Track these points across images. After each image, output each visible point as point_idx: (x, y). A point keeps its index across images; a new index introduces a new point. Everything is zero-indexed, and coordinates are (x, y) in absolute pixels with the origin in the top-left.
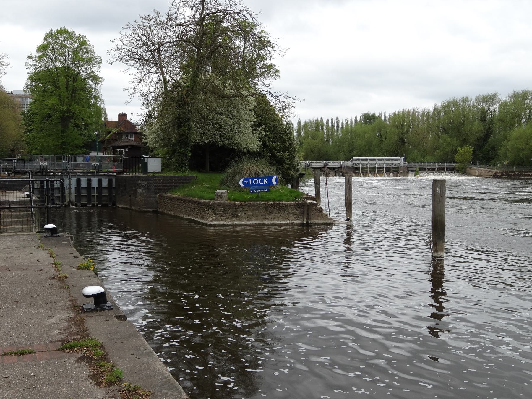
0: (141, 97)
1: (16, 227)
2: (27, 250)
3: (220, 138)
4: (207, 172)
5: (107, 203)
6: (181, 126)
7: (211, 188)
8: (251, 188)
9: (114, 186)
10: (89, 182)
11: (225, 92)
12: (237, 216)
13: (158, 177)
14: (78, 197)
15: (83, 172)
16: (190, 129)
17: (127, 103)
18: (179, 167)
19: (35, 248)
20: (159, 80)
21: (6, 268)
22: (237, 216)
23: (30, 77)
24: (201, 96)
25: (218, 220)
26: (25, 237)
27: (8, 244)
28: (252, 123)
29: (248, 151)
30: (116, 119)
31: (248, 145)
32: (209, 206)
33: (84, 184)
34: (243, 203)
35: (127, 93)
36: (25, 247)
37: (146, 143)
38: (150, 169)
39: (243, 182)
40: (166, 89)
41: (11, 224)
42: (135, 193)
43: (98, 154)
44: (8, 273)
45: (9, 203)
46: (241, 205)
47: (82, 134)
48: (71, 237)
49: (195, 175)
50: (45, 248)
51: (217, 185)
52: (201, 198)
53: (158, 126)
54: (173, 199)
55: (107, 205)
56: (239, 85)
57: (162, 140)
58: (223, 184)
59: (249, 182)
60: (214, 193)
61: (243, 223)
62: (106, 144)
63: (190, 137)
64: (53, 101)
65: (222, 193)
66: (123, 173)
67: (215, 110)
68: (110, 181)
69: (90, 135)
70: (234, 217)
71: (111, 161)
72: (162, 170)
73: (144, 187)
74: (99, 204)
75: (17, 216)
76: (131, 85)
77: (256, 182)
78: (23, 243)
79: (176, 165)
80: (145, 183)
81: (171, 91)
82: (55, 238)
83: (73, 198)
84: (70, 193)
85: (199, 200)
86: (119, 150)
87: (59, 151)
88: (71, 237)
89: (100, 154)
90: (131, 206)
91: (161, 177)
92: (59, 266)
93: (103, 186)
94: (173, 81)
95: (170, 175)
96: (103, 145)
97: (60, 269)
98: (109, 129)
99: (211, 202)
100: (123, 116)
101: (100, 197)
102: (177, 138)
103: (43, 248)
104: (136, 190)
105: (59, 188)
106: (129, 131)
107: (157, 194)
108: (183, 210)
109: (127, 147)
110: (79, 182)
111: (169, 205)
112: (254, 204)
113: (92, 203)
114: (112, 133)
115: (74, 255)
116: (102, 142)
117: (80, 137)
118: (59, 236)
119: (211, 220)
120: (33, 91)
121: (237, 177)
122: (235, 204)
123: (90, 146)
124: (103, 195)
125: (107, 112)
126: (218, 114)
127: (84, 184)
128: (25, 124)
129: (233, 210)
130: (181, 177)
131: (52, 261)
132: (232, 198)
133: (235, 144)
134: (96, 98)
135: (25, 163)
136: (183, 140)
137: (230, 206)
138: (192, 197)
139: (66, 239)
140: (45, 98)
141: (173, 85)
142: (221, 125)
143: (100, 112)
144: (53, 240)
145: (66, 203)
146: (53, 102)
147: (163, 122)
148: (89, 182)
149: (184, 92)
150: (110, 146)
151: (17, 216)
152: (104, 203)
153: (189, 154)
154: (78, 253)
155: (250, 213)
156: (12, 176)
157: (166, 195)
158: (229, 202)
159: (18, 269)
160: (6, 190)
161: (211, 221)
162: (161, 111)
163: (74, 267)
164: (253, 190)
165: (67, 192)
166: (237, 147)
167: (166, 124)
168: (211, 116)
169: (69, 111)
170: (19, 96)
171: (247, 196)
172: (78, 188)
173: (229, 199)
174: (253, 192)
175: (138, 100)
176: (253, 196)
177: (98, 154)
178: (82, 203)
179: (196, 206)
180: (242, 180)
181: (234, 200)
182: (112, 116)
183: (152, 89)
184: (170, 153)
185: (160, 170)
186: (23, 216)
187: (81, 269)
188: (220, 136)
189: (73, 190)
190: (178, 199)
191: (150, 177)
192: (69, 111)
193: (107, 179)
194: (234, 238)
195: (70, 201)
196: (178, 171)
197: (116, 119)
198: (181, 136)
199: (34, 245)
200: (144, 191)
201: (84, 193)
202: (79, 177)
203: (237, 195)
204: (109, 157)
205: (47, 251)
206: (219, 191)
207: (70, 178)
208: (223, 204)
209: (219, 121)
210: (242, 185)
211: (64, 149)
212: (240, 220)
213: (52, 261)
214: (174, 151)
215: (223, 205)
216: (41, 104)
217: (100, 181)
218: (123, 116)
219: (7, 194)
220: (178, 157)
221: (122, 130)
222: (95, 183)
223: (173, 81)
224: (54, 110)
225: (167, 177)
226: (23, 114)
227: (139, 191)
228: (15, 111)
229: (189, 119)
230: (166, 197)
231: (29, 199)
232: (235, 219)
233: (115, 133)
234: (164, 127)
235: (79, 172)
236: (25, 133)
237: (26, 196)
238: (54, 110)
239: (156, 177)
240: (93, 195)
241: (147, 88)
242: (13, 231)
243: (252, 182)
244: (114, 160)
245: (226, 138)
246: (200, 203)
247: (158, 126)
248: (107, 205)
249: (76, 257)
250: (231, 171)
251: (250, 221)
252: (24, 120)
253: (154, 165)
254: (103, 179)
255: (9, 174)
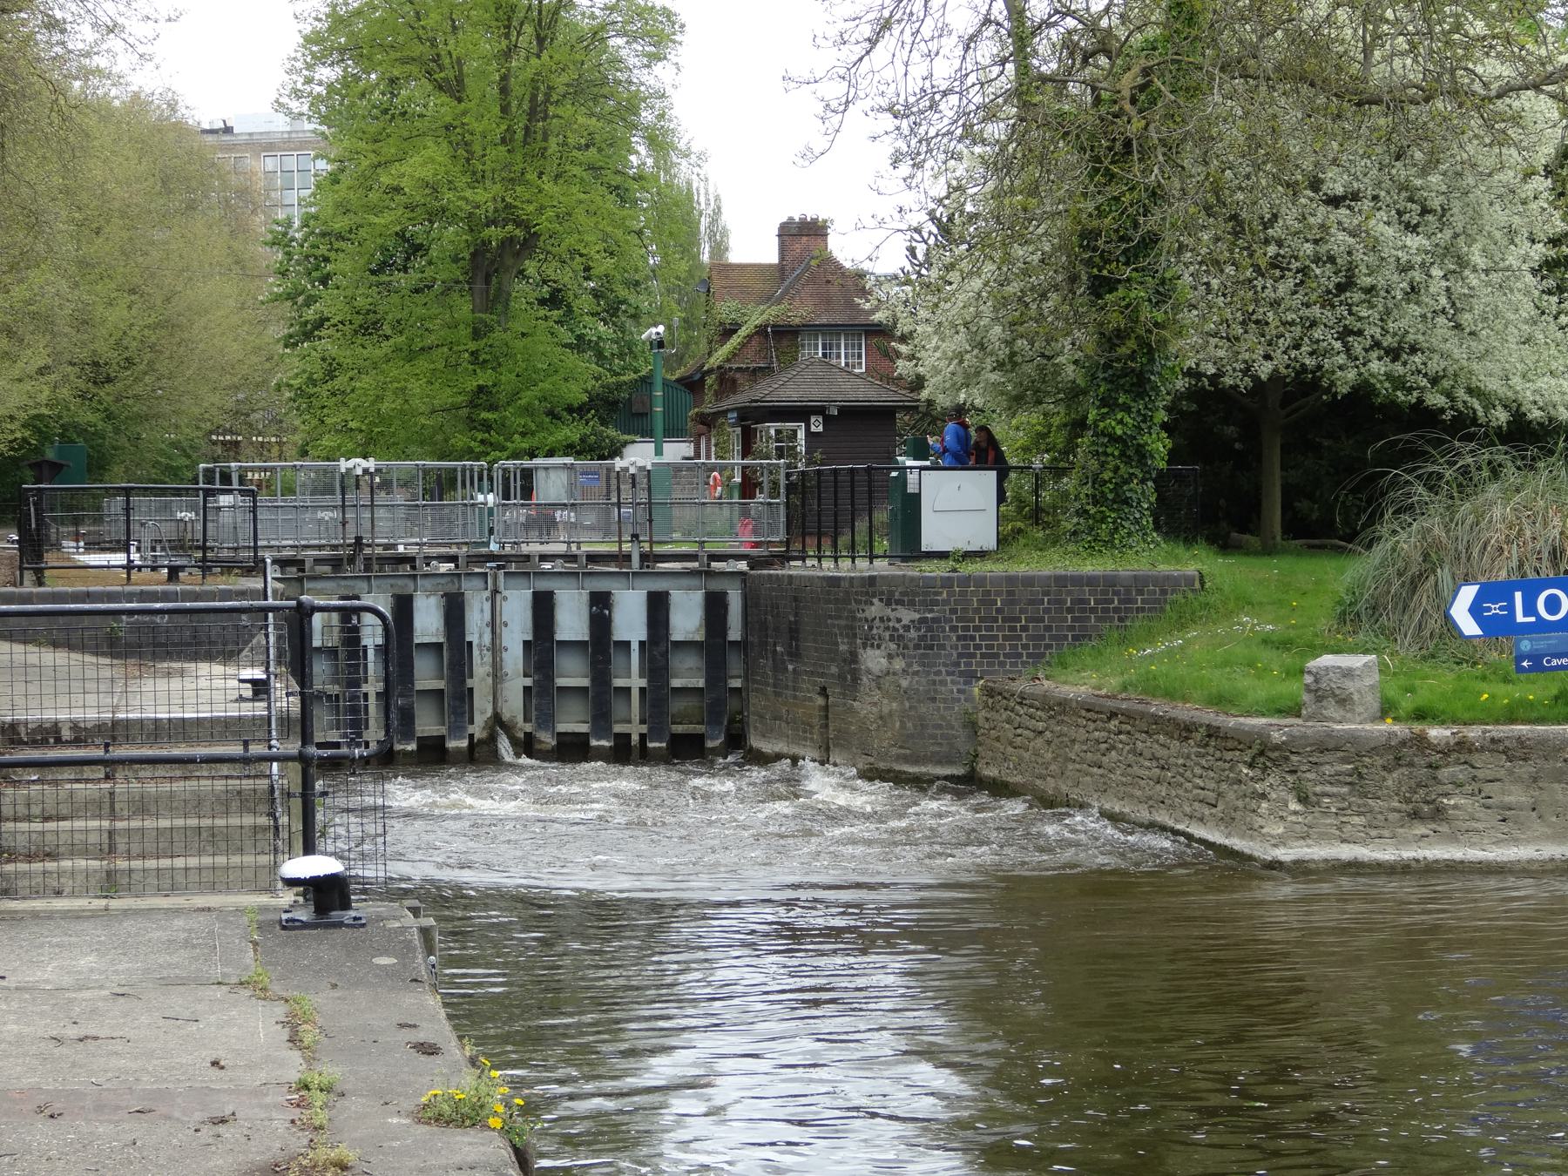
0: (888, 122)
1: (193, 862)
2: (177, 1001)
3: (1348, 349)
4: (1268, 551)
5: (700, 729)
6: (1110, 285)
7: (1284, 645)
8: (1526, 646)
9: (735, 634)
10: (601, 604)
11: (1379, 72)
12: (1438, 814)
13: (980, 582)
14: (542, 694)
15: (571, 558)
16: (1163, 293)
17: (809, 156)
18: (1102, 517)
19: (220, 992)
20: (987, 21)
21: (41, 1099)
22: (1438, 814)
23: (309, 40)
24: (1220, 101)
25: (1324, 837)
26: (179, 923)
27: (87, 961)
28: (1539, 251)
29: (1518, 418)
30: (769, 254)
31: (1516, 381)
32: (1265, 754)
33: (572, 623)
34: (1473, 733)
35: (806, 103)
36: (167, 983)
37: (919, 383)
38: (935, 533)
39: (1476, 610)
40: (1023, 69)
41: (167, 844)
42: (851, 675)
43: (659, 452)
44: (41, 1134)
45: (158, 730)
46: (1462, 746)
47: (580, 344)
48: (425, 932)
49: (1191, 569)
50: (276, 989)
51: (1323, 624)
52: (1220, 701)
53: (977, 283)
54: (1059, 708)
55: (699, 739)
56: (1457, 27)
57: (1000, 366)
58: (1357, 619)
59: (1511, 608)
60: (1302, 672)
61: (1474, 854)
62: (709, 396)
63: (1163, 342)
64: (425, 163)
65: (1348, 673)
66: (784, 558)
67: (1315, 184)
68: (715, 607)
69: (628, 349)
70: (1415, 815)
71: (728, 487)
72: (1002, 540)
73: (897, 638)
74: (655, 733)
75: (196, 804)
76: (830, 58)
77: (1553, 604)
78: (163, 959)
79: (1082, 513)
80: (907, 615)
81: (1057, 83)
82: (337, 935)
83: (513, 706)
84: (497, 674)
85: (1209, 716)
86: (772, 428)
87: (460, 441)
88: (425, 932)
89: (676, 451)
90: (246, 744)
91: (996, 581)
92: (319, 1098)
93: (677, 636)
94: (1071, 23)
95: (1047, 570)
96: (699, 398)
97: (321, 1118)
98: (726, 309)
99: (1279, 729)
100: (803, 235)
101: (657, 696)
102: (1091, 348)
103: (263, 993)
104: (853, 657)
105: (437, 647)
106: (839, 319)
107: (971, 676)
108: (1117, 776)
109: (820, 411)
110: (543, 607)
111: (1039, 742)
112: (1542, 742)
113: (618, 728)
114: (743, 332)
115: (420, 1036)
116: (693, 385)
117: (571, 358)
118: (357, 923)
119: (1280, 836)
120: (337, 108)
121: (1444, 574)
122: (1421, 741)
123: (620, 411)
124: (676, 683)
125: (727, 218)
126: (1334, 201)
127: (572, 623)
128: (291, 297)
129: (1414, 775)
130: (1110, 581)
131: (293, 1066)
132: (1407, 703)
133: (1435, 381)
134: (660, 142)
135: (254, 510)
136: (1125, 367)
137: (1396, 753)
138: (1170, 695)
139: (394, 942)
140: (389, 150)
141: (1069, 45)
142: (1351, 269)
143: (678, 217)
144: (325, 947)
145: (478, 729)
146: (427, 173)
147: (1007, 259)
148: (601, 604)
149: (1128, 81)
150: (725, 404)
151: (196, 804)
152: (679, 729)
153: (1159, 446)
154: (447, 1027)
155: (1517, 796)
156: (190, 581)
157: (1021, 686)
158: (1388, 726)
159: (99, 1108)
160: (155, 657)
161: (1281, 841)
162: (997, 195)
163: (408, 1105)
164: (1536, 658)
165: (481, 666)
166: (1449, 395)
167: (1026, 273)
168: (1290, 217)
169: (506, 213)
170: (265, 145)
171: (1501, 689)
172: (542, 645)
173: (1387, 709)
174: (1537, 667)
175: (867, 142)
176: (1535, 690)
177: (659, 452)
178: (562, 727)
179: (1191, 748)
180: (1468, 593)
181: (1421, 715)
182: (753, 244)
183: (944, 71)
184: (1059, 439)
185: (990, 542)
186: (224, 804)
187: (439, 1119)
188: (1345, 333)
189: (514, 657)
190: (1090, 710)
191: (929, 583)
192: (506, 213)
193: (698, 597)
194: (1419, 938)
195: (497, 720)
196: (1098, 544)
197: (769, 254)
198: (1109, 340)
199: (218, 972)
200: (898, 664)
201: (572, 674)
202: (543, 585)
203: (1437, 683)
204: (722, 469)
205: (280, 1010)
206: (1327, 660)
207: (496, 591)
208: (1353, 739)
209: (1339, 241)
210: (1469, 627)
211: (484, 428)
212: (1453, 838)
213: (293, 1066)
214: (1079, 426)
215: (1352, 750)
216: (365, 183)
217: (658, 606)
218: (803, 235)
219: (162, 684)
220: (1093, 464)
221: (799, 311)
222: (630, 622)
223: (1071, 23)
224: (438, 214)
225: (1029, 581)
226: (280, 241)
227: (873, 660)
228: (239, 230)
229: (1151, 240)
230: (1022, 699)
231: (259, 709)
232: (1421, 829)
233: (761, 331)
234: (1014, 288)
235: (544, 558)
236: (290, 342)
237: (248, 692)
238: (438, 214)
239: (966, 581)
240: (619, 682)
241: (919, 69)
242: (171, 884)
243: (1530, 609)
244: (748, 487)
245: (1377, 345)
246: (1213, 732)
247: (977, 283)
248: (699, 739)
249: (428, 1049)
250: (1400, 540)
251: (1516, 841)
252: (284, 274)
253: (957, 508)
254: (677, 597)
255: (174, 573)
